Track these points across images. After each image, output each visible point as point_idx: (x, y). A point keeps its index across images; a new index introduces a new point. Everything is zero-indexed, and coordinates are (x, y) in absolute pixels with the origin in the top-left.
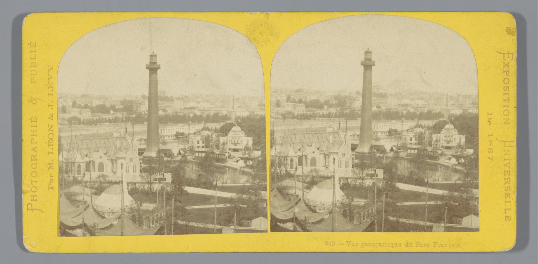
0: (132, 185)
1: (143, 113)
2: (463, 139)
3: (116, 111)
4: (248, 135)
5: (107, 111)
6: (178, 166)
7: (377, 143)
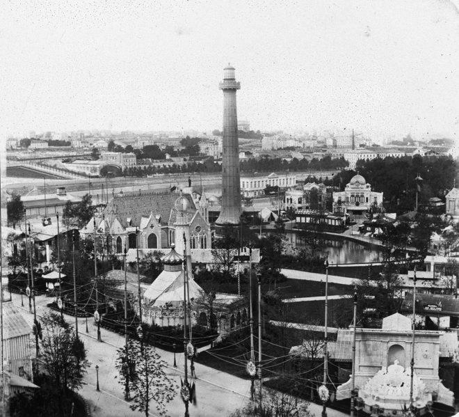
0: (200, 268)
1: (215, 158)
2: (380, 197)
3: (174, 154)
4: (375, 188)
5: (161, 156)
6: (271, 238)
7: (249, 209)
